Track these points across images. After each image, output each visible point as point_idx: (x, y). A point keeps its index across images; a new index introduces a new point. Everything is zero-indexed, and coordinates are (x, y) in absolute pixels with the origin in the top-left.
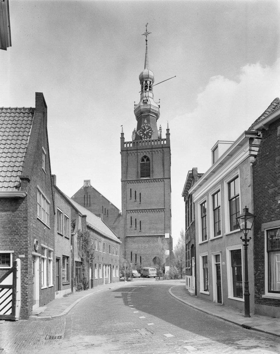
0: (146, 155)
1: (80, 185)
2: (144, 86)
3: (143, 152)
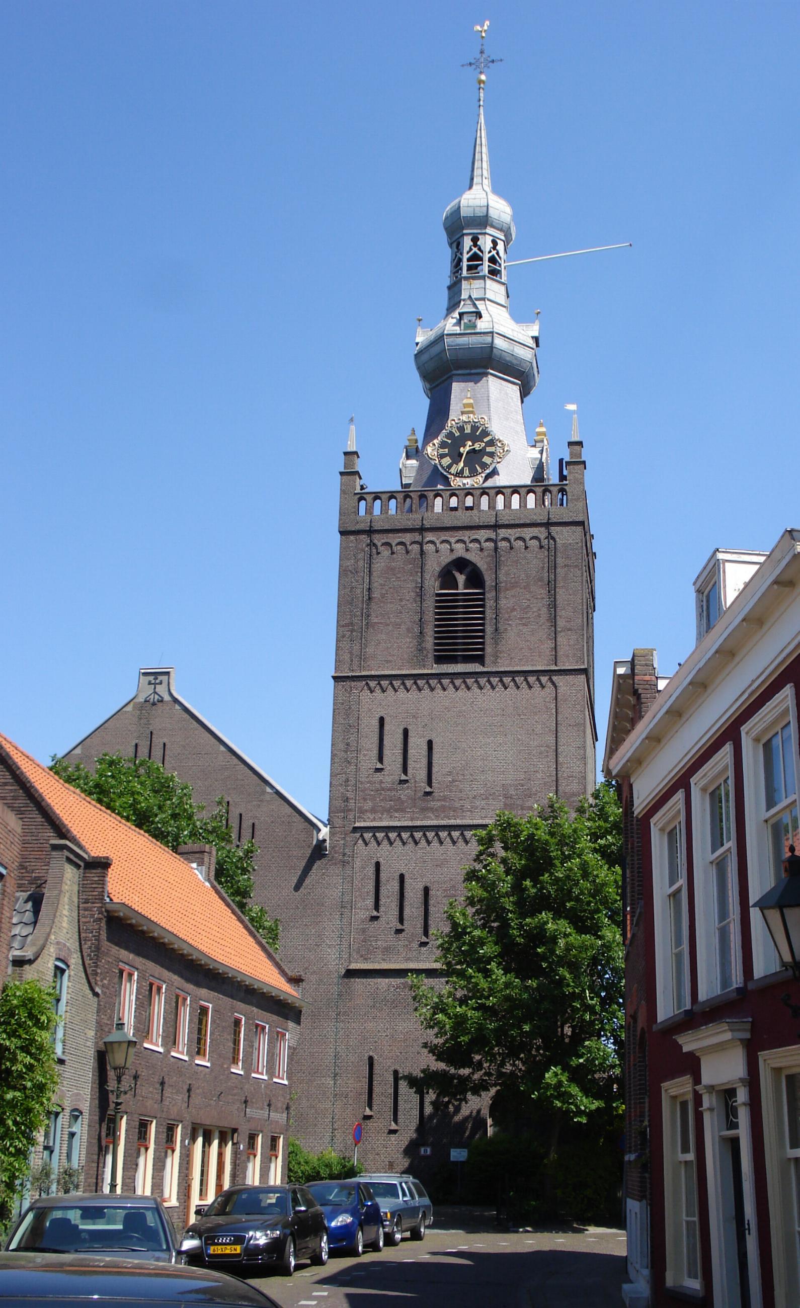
0: (468, 556)
1: (112, 692)
2: (465, 257)
3: (453, 540)
